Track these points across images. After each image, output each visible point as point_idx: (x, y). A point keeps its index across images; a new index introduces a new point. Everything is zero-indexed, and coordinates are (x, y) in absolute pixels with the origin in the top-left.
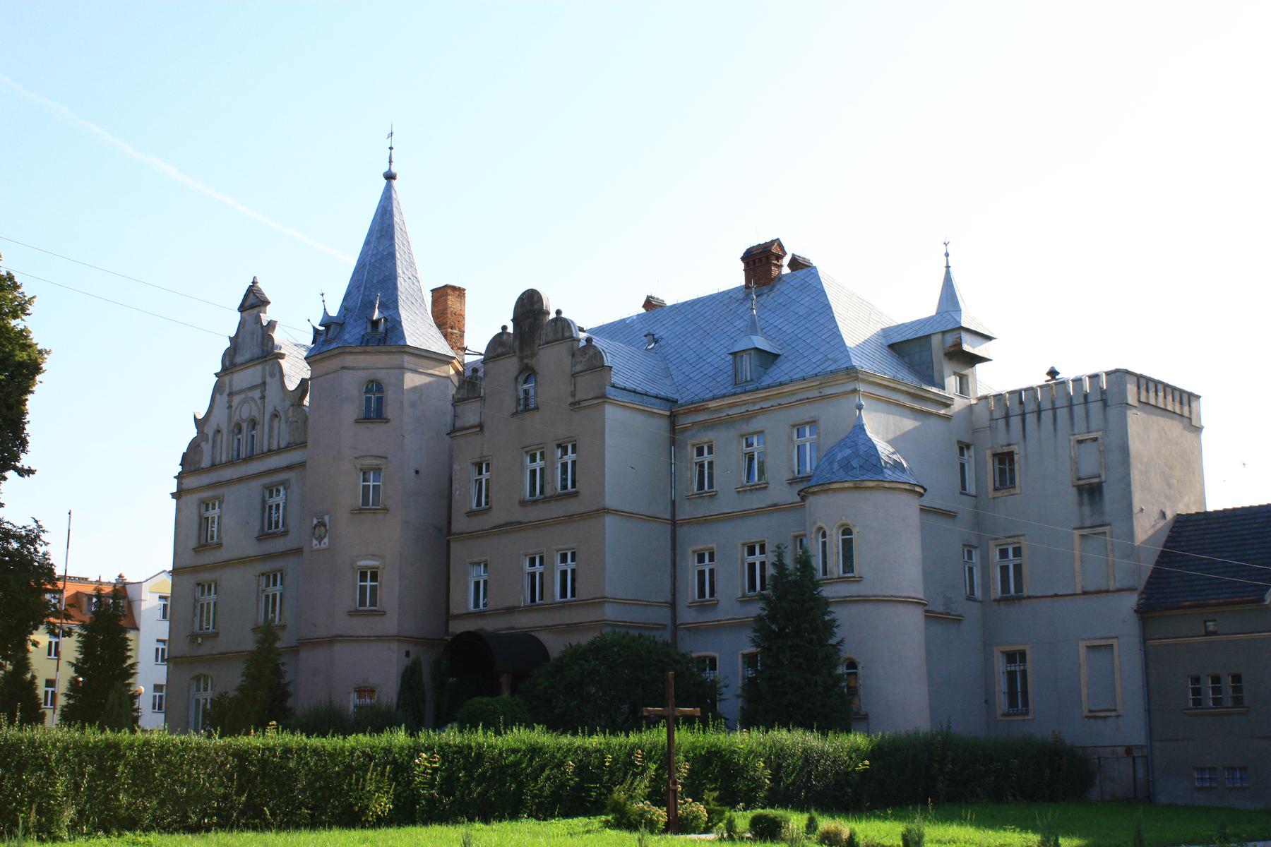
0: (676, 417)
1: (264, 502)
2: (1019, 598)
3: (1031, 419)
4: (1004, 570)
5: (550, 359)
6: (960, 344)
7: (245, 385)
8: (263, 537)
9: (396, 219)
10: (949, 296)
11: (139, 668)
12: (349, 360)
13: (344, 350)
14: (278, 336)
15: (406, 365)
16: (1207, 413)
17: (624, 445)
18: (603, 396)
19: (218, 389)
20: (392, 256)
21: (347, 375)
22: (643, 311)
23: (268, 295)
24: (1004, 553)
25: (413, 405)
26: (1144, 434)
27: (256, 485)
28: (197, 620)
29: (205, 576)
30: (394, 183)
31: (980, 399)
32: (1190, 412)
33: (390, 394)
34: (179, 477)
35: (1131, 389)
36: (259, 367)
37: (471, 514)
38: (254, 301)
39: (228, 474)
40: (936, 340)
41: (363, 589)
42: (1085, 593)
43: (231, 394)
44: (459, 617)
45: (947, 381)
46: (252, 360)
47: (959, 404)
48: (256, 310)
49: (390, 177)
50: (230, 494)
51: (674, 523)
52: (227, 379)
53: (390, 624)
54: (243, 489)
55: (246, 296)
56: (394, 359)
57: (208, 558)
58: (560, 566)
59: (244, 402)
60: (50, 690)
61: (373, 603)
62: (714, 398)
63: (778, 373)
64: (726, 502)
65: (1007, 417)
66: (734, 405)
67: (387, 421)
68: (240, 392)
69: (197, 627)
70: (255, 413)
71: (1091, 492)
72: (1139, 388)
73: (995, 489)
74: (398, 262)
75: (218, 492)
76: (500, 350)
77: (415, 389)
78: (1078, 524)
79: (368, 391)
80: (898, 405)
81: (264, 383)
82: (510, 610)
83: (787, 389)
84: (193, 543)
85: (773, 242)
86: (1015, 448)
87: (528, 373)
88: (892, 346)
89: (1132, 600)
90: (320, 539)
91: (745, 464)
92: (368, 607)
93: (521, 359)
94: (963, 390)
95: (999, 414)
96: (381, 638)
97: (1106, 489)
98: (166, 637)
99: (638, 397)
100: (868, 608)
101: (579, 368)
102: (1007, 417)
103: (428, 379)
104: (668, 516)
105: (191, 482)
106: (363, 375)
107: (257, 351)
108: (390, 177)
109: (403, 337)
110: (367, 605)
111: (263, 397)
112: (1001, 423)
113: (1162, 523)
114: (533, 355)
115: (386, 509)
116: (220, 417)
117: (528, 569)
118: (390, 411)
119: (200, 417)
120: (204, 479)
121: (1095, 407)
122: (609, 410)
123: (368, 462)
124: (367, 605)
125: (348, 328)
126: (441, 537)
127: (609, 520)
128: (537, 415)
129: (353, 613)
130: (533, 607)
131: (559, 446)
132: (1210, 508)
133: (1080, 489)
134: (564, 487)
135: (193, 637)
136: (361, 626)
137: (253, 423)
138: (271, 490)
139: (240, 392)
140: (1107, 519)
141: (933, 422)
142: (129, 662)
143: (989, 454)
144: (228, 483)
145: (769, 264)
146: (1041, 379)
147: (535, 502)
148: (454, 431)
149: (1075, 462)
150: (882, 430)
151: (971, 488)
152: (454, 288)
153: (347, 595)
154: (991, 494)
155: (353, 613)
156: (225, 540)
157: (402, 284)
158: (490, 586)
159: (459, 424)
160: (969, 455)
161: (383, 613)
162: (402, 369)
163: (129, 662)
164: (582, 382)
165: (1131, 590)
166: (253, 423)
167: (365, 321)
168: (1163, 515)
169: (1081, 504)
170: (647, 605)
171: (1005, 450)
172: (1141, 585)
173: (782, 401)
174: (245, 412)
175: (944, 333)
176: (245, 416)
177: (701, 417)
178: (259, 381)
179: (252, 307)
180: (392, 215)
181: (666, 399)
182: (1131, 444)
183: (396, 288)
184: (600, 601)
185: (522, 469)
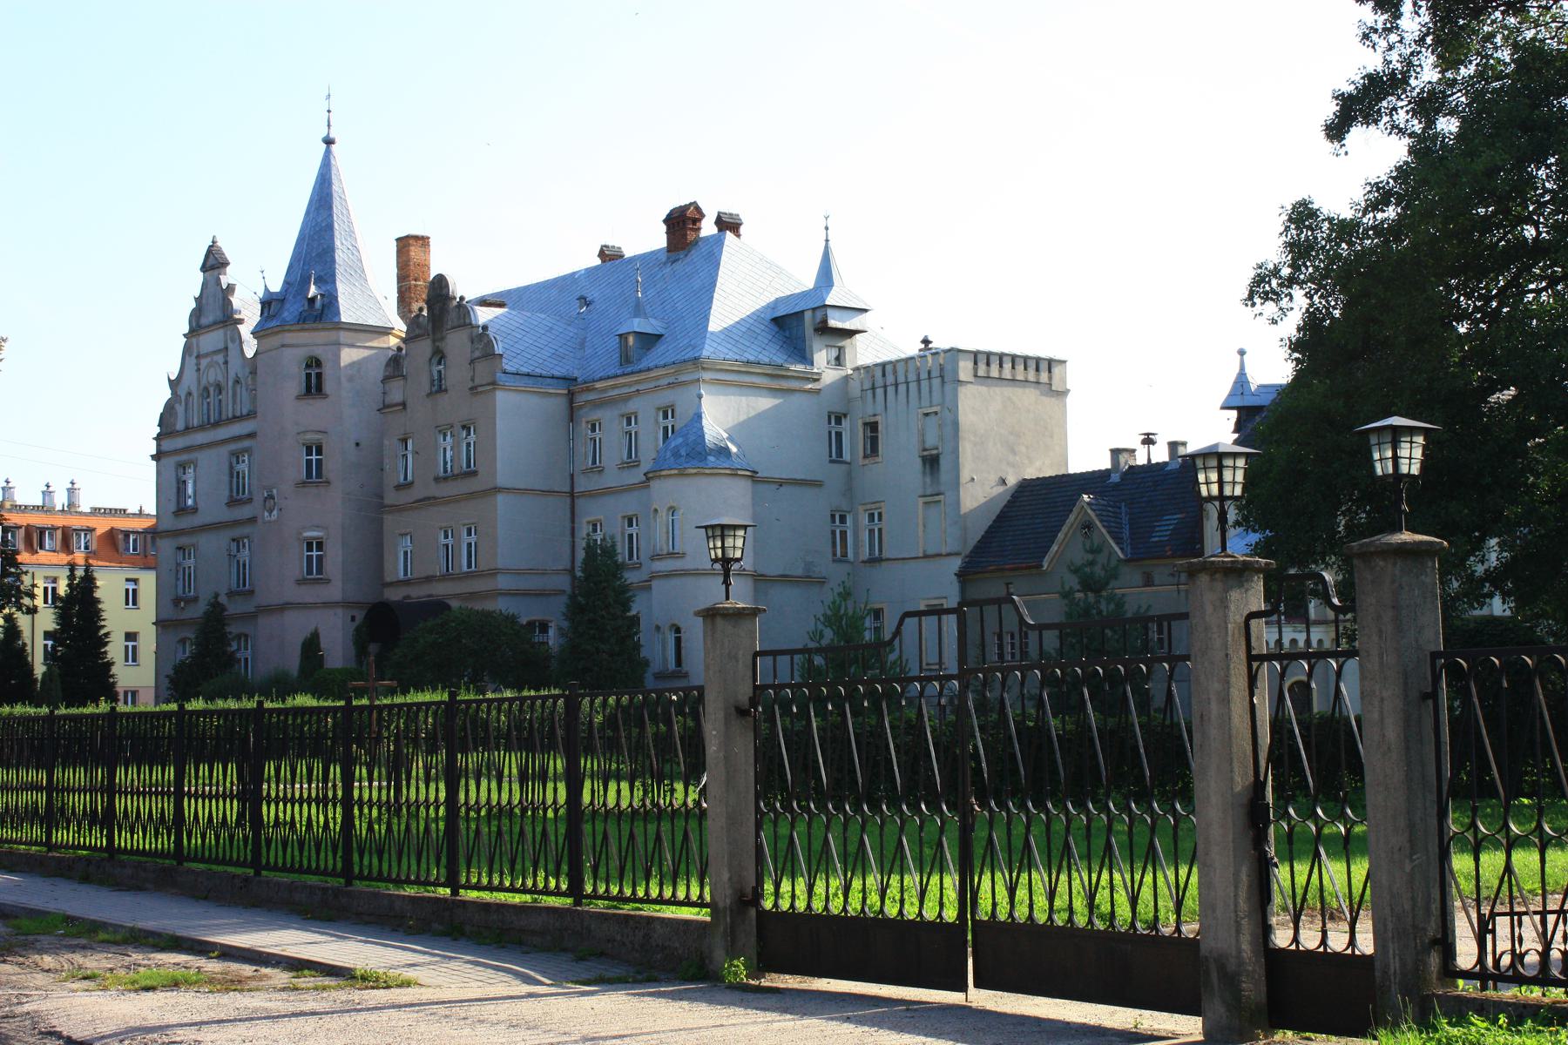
0: (573, 393)
1: (231, 467)
2: (880, 560)
3: (891, 390)
4: (871, 532)
5: (456, 343)
6: (825, 321)
7: (211, 349)
8: (233, 502)
9: (335, 188)
10: (826, 275)
11: (112, 637)
12: (290, 338)
13: (283, 328)
14: (236, 301)
15: (342, 340)
16: (1074, 378)
17: (516, 427)
18: (494, 383)
19: (187, 350)
20: (330, 227)
21: (288, 352)
22: (598, 262)
23: (229, 255)
24: (871, 516)
25: (351, 379)
26: (977, 407)
27: (224, 451)
28: (180, 583)
29: (184, 541)
30: (333, 147)
31: (857, 369)
32: (1050, 378)
33: (327, 370)
34: (158, 438)
35: (965, 369)
36: (221, 332)
37: (399, 487)
38: (214, 262)
39: (200, 438)
40: (808, 315)
41: (310, 558)
42: (926, 557)
43: (198, 357)
44: (391, 584)
45: (816, 357)
46: (215, 323)
47: (830, 376)
48: (216, 272)
49: (329, 142)
50: (203, 457)
51: (572, 495)
52: (194, 340)
53: (334, 592)
54: (212, 452)
55: (207, 257)
56: (332, 336)
57: (185, 522)
58: (465, 539)
59: (209, 366)
60: (130, 644)
61: (320, 571)
62: (601, 379)
63: (658, 355)
64: (612, 478)
65: (873, 388)
66: (614, 387)
67: (326, 396)
68: (207, 355)
69: (180, 592)
70: (220, 378)
71: (931, 462)
72: (976, 363)
73: (865, 457)
74: (337, 234)
75: (192, 456)
76: (417, 332)
77: (352, 365)
78: (920, 492)
79: (308, 366)
80: (741, 386)
81: (226, 348)
82: (429, 579)
83: (653, 374)
84: (173, 507)
85: (687, 207)
86: (878, 418)
87: (439, 355)
88: (775, 320)
89: (956, 564)
90: (271, 511)
91: (625, 441)
92: (315, 576)
93: (434, 341)
94: (839, 361)
95: (867, 385)
96: (327, 605)
97: (942, 461)
98: (1153, 461)
99: (531, 381)
100: (690, 581)
101: (477, 354)
102: (873, 388)
103: (366, 353)
104: (567, 489)
105: (168, 445)
106: (302, 353)
107: (219, 315)
108: (329, 142)
109: (338, 313)
110: (315, 572)
111: (226, 363)
112: (869, 393)
113: (1001, 489)
114: (443, 339)
115: (328, 482)
116: (190, 381)
117: (442, 540)
118: (328, 386)
119: (173, 378)
120: (180, 442)
121: (936, 382)
122: (500, 396)
123: (310, 437)
124: (315, 572)
125: (287, 306)
126: (376, 509)
127: (500, 498)
128: (446, 397)
129: (301, 582)
130: (447, 577)
131: (464, 427)
132: (1071, 471)
133: (924, 459)
134: (469, 465)
135: (176, 601)
136: (309, 594)
137: (219, 389)
138: (236, 455)
139: (207, 355)
140: (942, 489)
141: (796, 399)
142: (102, 632)
143: (860, 422)
144: (201, 447)
145: (684, 228)
146: (913, 348)
147: (445, 479)
148: (385, 407)
149: (923, 435)
150: (720, 415)
151: (847, 456)
152: (416, 238)
153: (294, 563)
154: (861, 461)
155: (301, 582)
156: (201, 505)
157: (340, 256)
158: (413, 557)
159: (388, 401)
160: (846, 423)
161: (328, 581)
162: (338, 345)
163: (102, 632)
164: (479, 366)
165: (957, 554)
166: (219, 389)
167: (306, 298)
168: (1003, 482)
169: (924, 473)
170: (543, 573)
171: (873, 419)
172: (967, 552)
173: (640, 387)
174: (213, 376)
175: (814, 309)
176: (211, 380)
177: (591, 396)
178: (221, 346)
179: (213, 268)
180: (330, 184)
181: (564, 378)
182: (962, 418)
183: (333, 261)
184: (493, 573)
185: (436, 448)
